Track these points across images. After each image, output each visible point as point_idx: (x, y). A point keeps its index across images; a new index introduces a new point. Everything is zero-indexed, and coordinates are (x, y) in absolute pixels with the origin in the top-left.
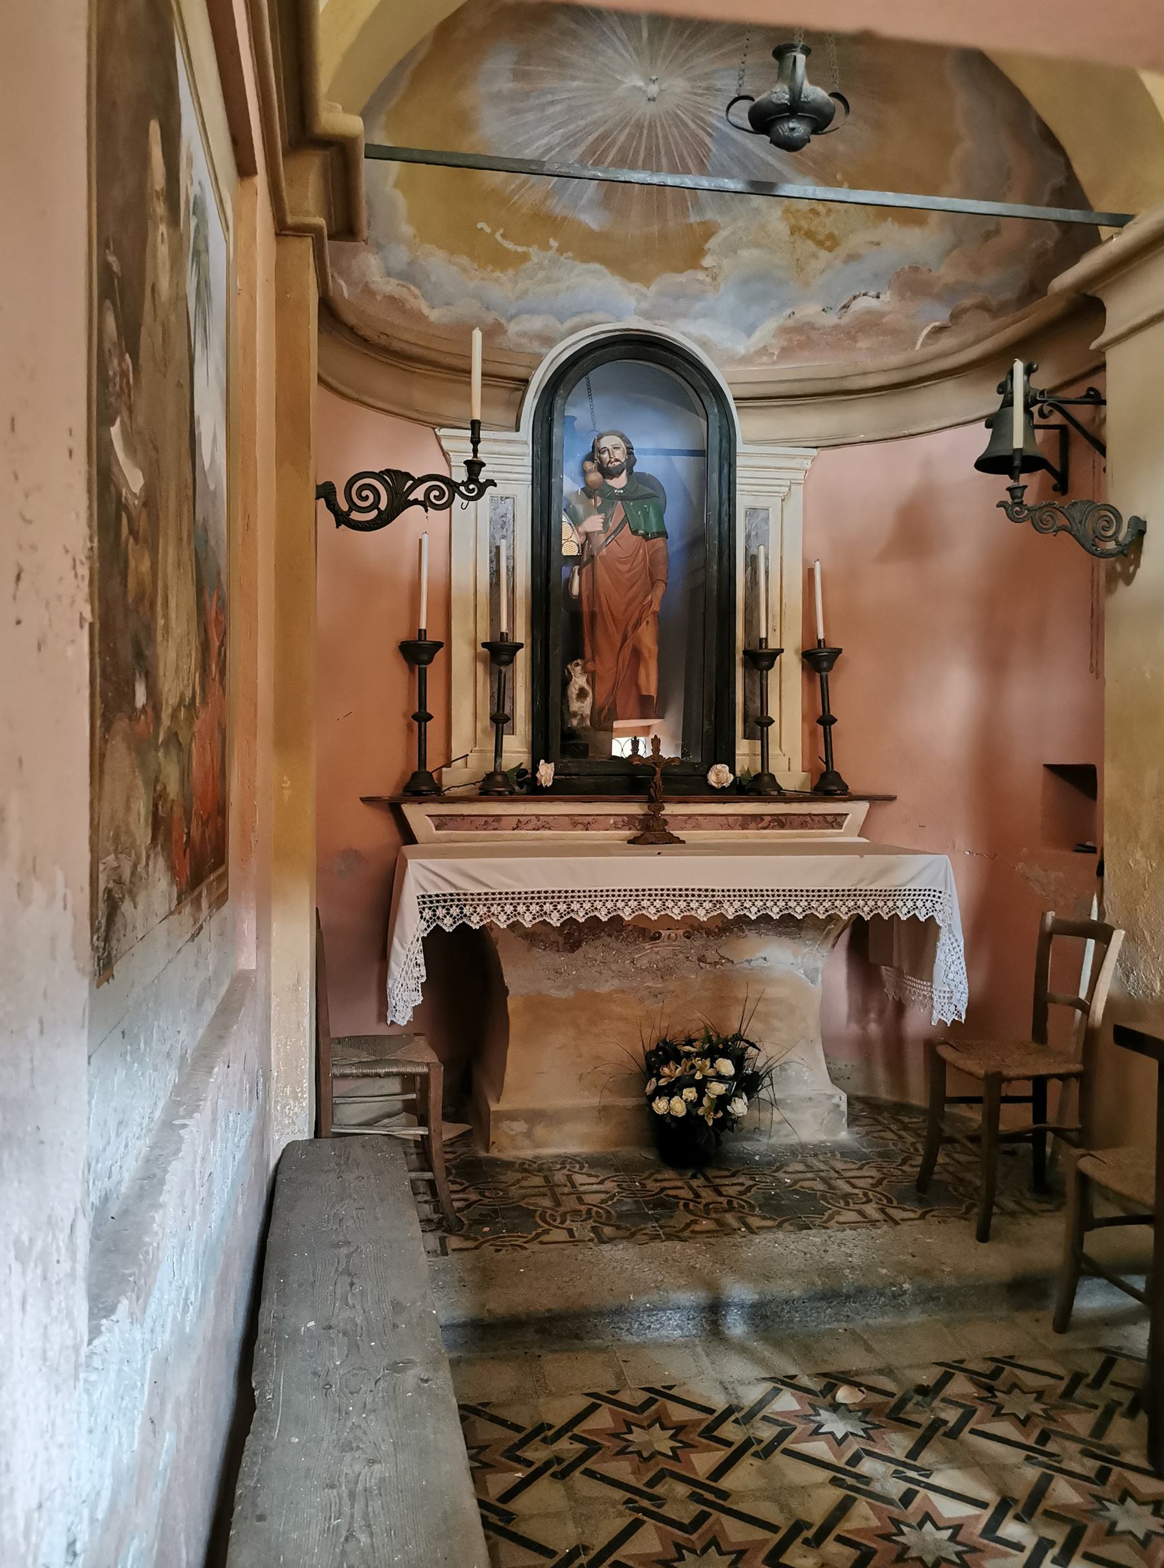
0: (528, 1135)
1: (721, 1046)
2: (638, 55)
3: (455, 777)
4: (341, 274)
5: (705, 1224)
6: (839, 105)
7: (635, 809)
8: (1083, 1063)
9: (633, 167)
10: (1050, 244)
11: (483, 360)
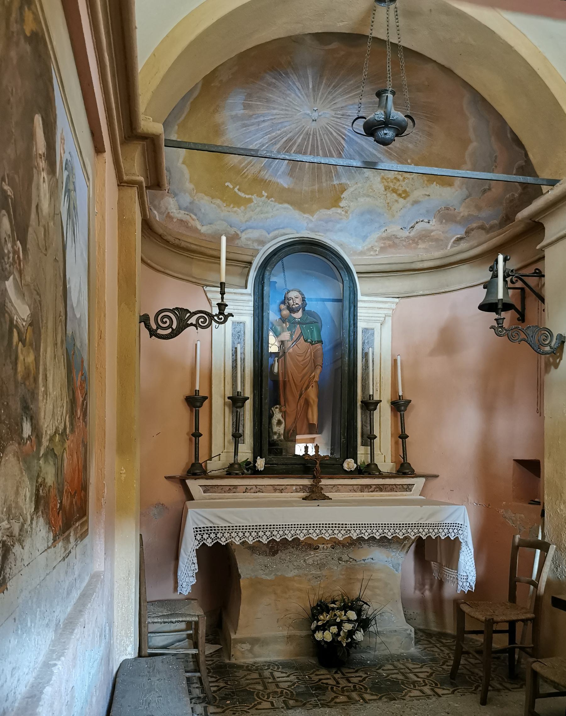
0: (251, 651)
1: (350, 604)
2: (307, 96)
3: (214, 466)
4: (155, 207)
5: (342, 698)
6: (410, 121)
7: (306, 482)
8: (534, 613)
9: (305, 153)
10: (516, 195)
11: (227, 252)
